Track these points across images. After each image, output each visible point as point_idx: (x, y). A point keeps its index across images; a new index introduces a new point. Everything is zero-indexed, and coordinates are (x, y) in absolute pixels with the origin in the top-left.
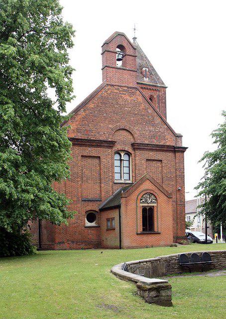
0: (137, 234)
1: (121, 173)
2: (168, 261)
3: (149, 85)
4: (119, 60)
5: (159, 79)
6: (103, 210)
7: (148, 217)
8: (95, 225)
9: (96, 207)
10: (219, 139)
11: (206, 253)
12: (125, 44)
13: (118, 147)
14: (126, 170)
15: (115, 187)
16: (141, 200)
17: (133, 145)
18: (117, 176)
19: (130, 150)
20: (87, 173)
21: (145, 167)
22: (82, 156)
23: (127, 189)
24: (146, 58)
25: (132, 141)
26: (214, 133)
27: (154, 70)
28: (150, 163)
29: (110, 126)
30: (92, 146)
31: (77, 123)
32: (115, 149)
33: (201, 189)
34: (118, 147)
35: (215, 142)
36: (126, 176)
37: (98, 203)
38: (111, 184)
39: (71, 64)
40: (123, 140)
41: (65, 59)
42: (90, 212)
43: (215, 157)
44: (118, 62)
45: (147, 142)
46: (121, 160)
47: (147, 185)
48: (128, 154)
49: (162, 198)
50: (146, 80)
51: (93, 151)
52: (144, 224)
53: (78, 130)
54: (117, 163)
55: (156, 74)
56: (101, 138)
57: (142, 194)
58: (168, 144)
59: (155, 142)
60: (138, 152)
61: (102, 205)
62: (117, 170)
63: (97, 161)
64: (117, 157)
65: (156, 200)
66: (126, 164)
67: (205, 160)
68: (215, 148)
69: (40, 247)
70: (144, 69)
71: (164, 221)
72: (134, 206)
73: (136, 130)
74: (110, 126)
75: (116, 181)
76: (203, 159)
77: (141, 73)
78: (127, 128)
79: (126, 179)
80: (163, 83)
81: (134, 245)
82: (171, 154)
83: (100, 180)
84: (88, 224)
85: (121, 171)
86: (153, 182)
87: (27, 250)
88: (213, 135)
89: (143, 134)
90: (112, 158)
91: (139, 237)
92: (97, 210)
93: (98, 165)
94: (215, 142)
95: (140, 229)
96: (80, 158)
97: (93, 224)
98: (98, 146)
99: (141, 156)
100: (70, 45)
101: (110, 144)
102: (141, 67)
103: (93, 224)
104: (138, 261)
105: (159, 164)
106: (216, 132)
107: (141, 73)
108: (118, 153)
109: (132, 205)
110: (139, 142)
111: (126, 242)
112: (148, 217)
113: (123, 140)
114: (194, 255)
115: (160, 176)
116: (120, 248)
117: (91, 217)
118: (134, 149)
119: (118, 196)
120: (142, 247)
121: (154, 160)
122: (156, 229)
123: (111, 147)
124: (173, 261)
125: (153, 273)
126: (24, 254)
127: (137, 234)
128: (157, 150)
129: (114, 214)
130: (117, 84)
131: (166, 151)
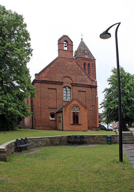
0: (70, 125)
1: (66, 97)
2: (60, 139)
3: (88, 59)
4: (65, 47)
5: (92, 56)
6: (57, 113)
7: (76, 119)
8: (54, 119)
9: (54, 111)
10: (111, 82)
11: (75, 136)
12: (68, 40)
13: (65, 85)
14: (69, 95)
15: (64, 103)
16: (72, 109)
17: (72, 84)
18: (65, 98)
19: (71, 86)
20: (50, 96)
21: (77, 94)
22: (48, 88)
23: (69, 103)
24: (87, 47)
25: (71, 82)
26: (108, 79)
27: (90, 52)
28: (80, 92)
29: (61, 75)
30: (53, 84)
31: (46, 74)
32: (63, 85)
33: (102, 105)
34: (65, 85)
35: (109, 84)
36: (69, 98)
37: (56, 109)
38: (61, 101)
39: (32, 47)
40: (67, 82)
41: (29, 45)
42: (51, 114)
43: (109, 90)
44: (64, 48)
45: (78, 83)
46: (66, 91)
47: (75, 102)
48: (70, 88)
49: (82, 109)
50: (86, 56)
51: (53, 86)
52: (74, 120)
53: (46, 77)
54: (65, 92)
55: (91, 54)
56: (57, 81)
57: (72, 107)
58: (88, 84)
59: (82, 83)
60: (74, 87)
61: (58, 110)
62: (65, 95)
63: (55, 91)
64: (65, 89)
65: (79, 109)
66: (69, 92)
67: (105, 92)
68: (109, 87)
69: (33, 127)
70: (85, 52)
71: (83, 119)
72: (68, 112)
73: (73, 77)
74: (61, 75)
75: (64, 100)
76: (104, 92)
77: (84, 53)
78: (69, 76)
79: (69, 99)
80: (94, 58)
81: (69, 129)
82: (89, 89)
83: (57, 99)
84: (51, 119)
85: (67, 95)
86: (78, 101)
87: (11, 128)
88: (108, 81)
89: (78, 79)
90: (62, 90)
91: (71, 126)
92: (55, 113)
93: (55, 93)
94: (109, 84)
95: (72, 123)
96: (47, 89)
97: (53, 119)
98: (55, 84)
99: (76, 89)
100: (30, 39)
101: (61, 83)
102: (84, 51)
103: (53, 119)
104: (40, 137)
105: (84, 93)
106: (110, 79)
107: (84, 53)
108: (65, 87)
109: (68, 111)
110: (74, 82)
111: (65, 128)
112: (76, 119)
113: (67, 82)
114: (75, 136)
115: (85, 99)
116: (63, 130)
117: (52, 116)
118: (72, 86)
119: (63, 107)
120: (72, 131)
121: (82, 91)
122: (79, 123)
123: (61, 85)
124: (64, 139)
125: (51, 143)
126: (10, 130)
127: (70, 125)
128: (83, 87)
129: (60, 115)
130: (65, 57)
131: (87, 87)
